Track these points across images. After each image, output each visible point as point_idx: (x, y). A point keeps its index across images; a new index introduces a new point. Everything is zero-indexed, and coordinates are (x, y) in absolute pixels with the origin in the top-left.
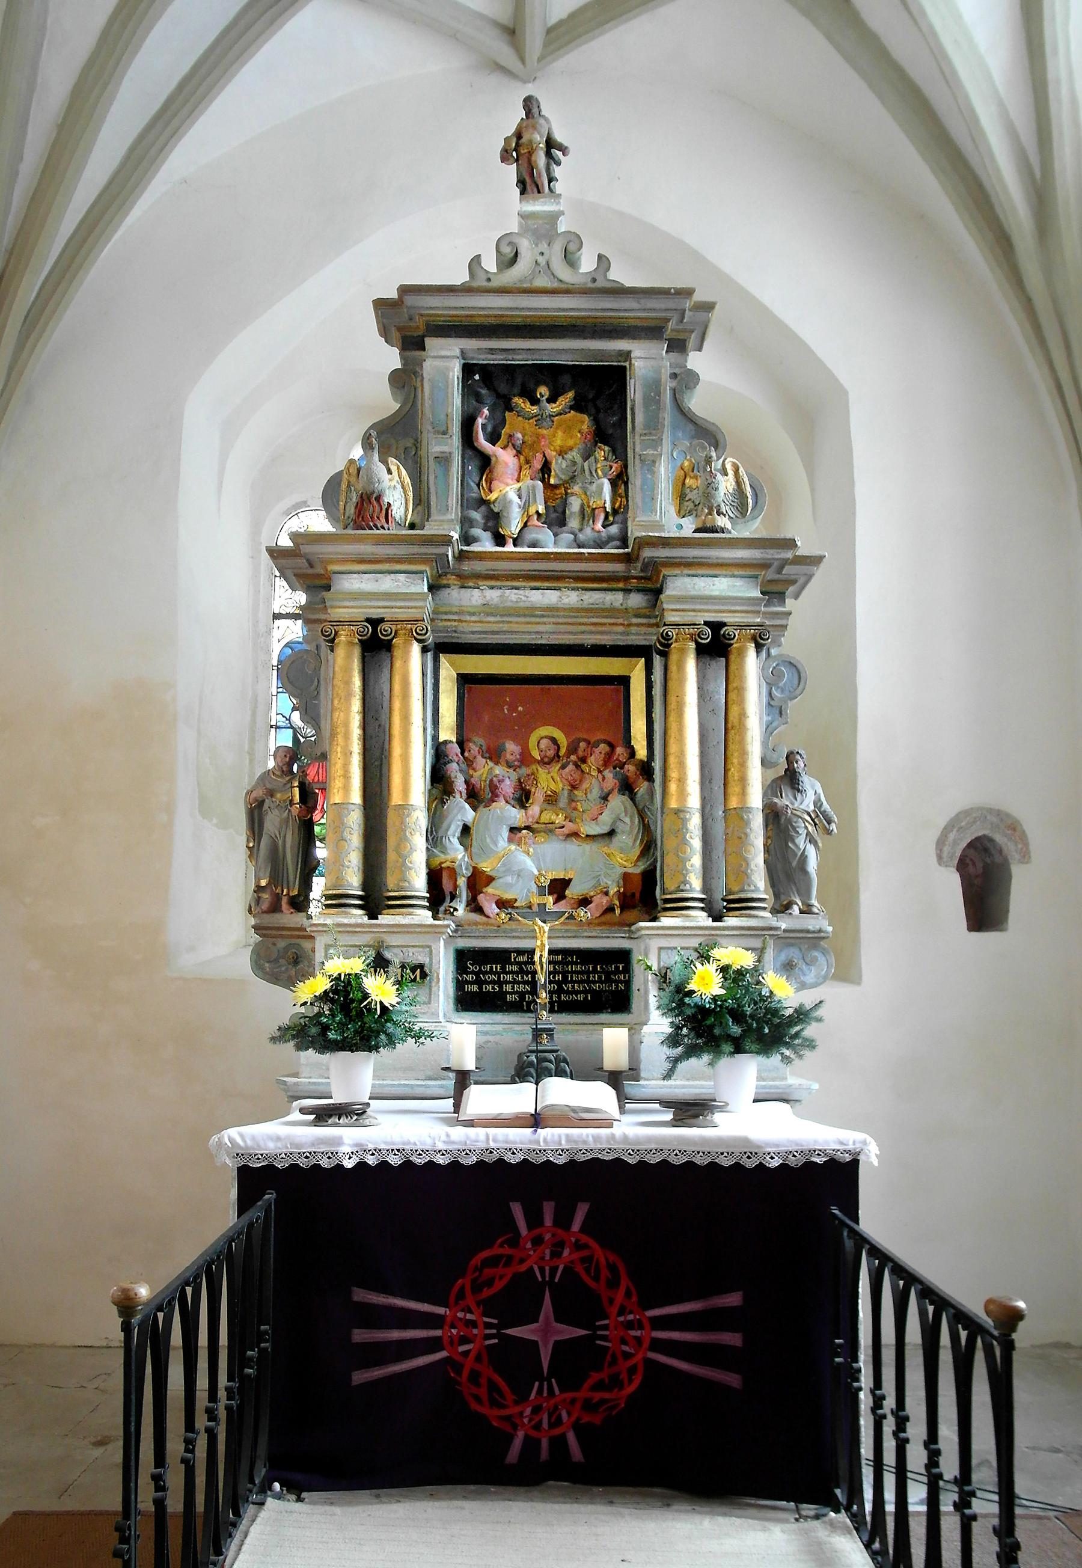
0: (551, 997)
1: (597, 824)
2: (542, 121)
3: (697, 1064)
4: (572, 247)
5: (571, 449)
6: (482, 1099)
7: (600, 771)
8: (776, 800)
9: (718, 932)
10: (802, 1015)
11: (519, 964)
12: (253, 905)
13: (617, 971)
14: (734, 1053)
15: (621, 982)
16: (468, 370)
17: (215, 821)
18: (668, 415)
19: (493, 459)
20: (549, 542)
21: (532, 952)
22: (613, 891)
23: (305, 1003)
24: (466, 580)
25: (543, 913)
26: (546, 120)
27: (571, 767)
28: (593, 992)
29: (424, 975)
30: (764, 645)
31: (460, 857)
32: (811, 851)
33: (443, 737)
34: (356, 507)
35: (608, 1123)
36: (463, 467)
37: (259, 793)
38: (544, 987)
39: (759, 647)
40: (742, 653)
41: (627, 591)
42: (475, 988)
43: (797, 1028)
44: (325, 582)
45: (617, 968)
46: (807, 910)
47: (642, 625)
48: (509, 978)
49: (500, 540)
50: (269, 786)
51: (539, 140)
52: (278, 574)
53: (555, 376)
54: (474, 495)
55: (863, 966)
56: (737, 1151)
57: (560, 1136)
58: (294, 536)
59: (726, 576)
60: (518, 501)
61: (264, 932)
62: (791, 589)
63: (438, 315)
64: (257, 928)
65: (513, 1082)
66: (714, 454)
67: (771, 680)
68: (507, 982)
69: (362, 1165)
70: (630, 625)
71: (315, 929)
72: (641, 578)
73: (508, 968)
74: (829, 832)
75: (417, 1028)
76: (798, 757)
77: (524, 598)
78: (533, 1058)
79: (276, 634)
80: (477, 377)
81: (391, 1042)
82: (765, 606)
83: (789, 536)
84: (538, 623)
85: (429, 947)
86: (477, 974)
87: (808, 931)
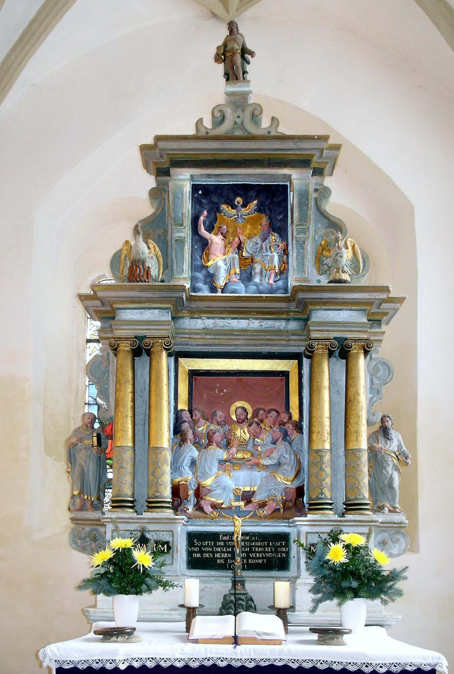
1: (270, 459)
2: (239, 36)
3: (331, 604)
4: (257, 112)
5: (255, 235)
6: (203, 626)
7: (271, 427)
8: (375, 445)
9: (341, 523)
10: (394, 576)
11: (224, 541)
12: (71, 506)
13: (281, 546)
14: (353, 598)
15: (284, 552)
16: (195, 188)
17: (54, 457)
18: (312, 213)
19: (210, 241)
20: (242, 290)
22: (279, 497)
23: (99, 566)
24: (195, 313)
25: (238, 512)
26: (242, 35)
27: (254, 425)
29: (169, 548)
30: (369, 351)
31: (190, 478)
32: (396, 475)
33: (180, 407)
34: (129, 270)
35: (278, 642)
36: (192, 247)
37: (74, 440)
38: (239, 555)
39: (366, 353)
40: (357, 356)
41: (288, 320)
42: (199, 555)
43: (391, 583)
44: (112, 315)
46: (393, 511)
47: (297, 340)
48: (219, 549)
49: (213, 289)
50: (79, 436)
51: (237, 47)
52: (89, 317)
53: (245, 191)
54: (198, 263)
55: (420, 542)
56: (359, 662)
57: (250, 650)
58: (93, 287)
59: (346, 310)
60: (224, 266)
61: (77, 522)
62: (385, 318)
63: (178, 154)
64: (73, 519)
65: (221, 614)
66: (340, 236)
67: (372, 373)
68: (218, 552)
69: (130, 668)
70: (289, 340)
71: (105, 520)
72: (296, 312)
73: (219, 543)
74: (407, 464)
75: (164, 580)
76: (388, 419)
77: (227, 325)
78: (233, 598)
79: (88, 351)
80: (200, 192)
81: (149, 590)
82: (370, 328)
83: (385, 285)
84: (236, 339)
85: (172, 531)
86: (200, 547)
87: (394, 523)
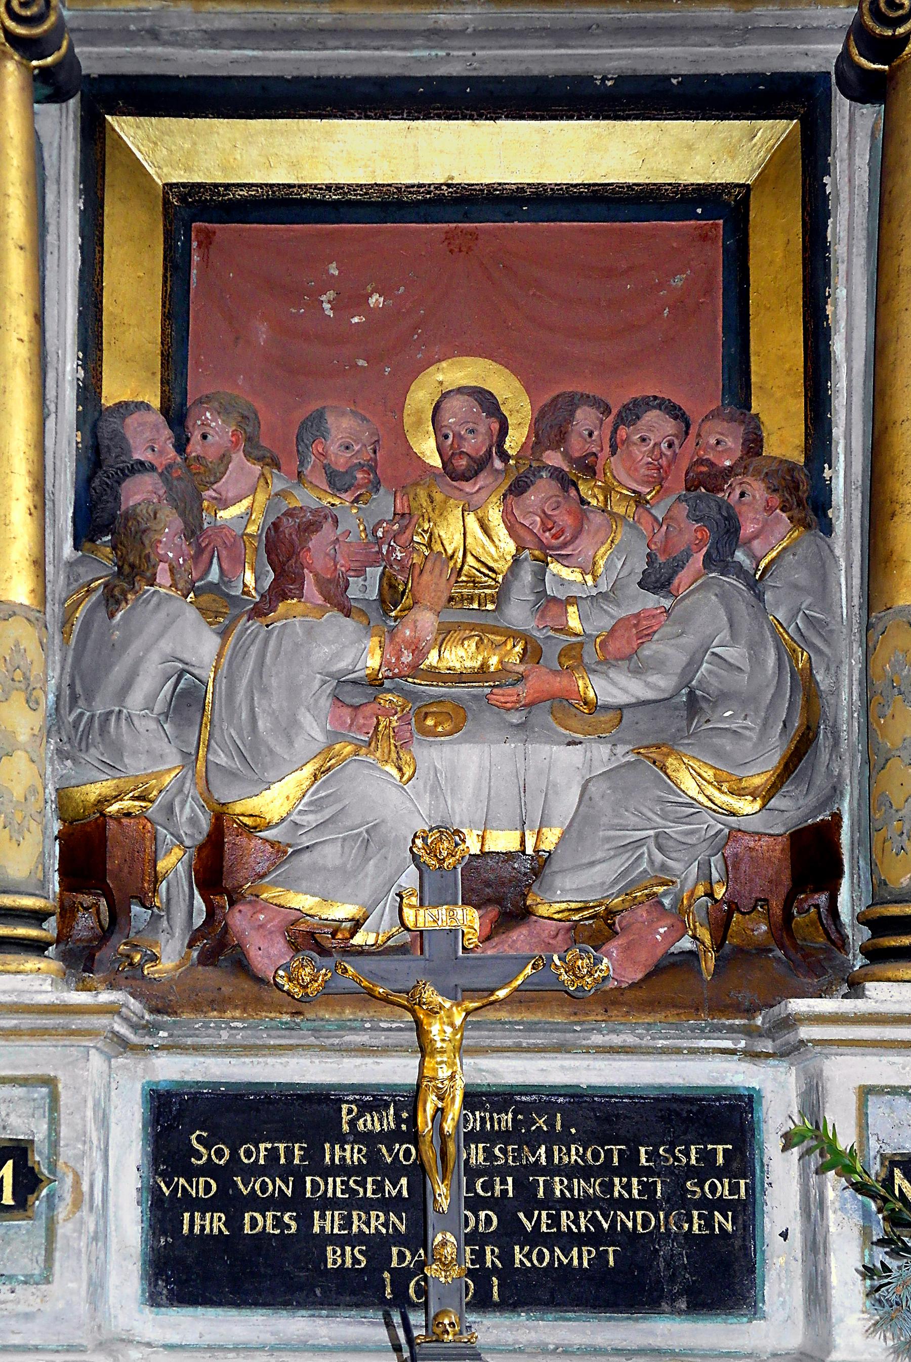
0: (479, 1257)
11: (368, 1139)
13: (707, 1169)
15: (723, 1206)
21: (411, 1099)
28: (629, 1240)
38: (448, 1222)
42: (215, 1223)
45: (707, 1157)
48: (334, 1187)
73: (333, 1154)
85: (49, 1082)
